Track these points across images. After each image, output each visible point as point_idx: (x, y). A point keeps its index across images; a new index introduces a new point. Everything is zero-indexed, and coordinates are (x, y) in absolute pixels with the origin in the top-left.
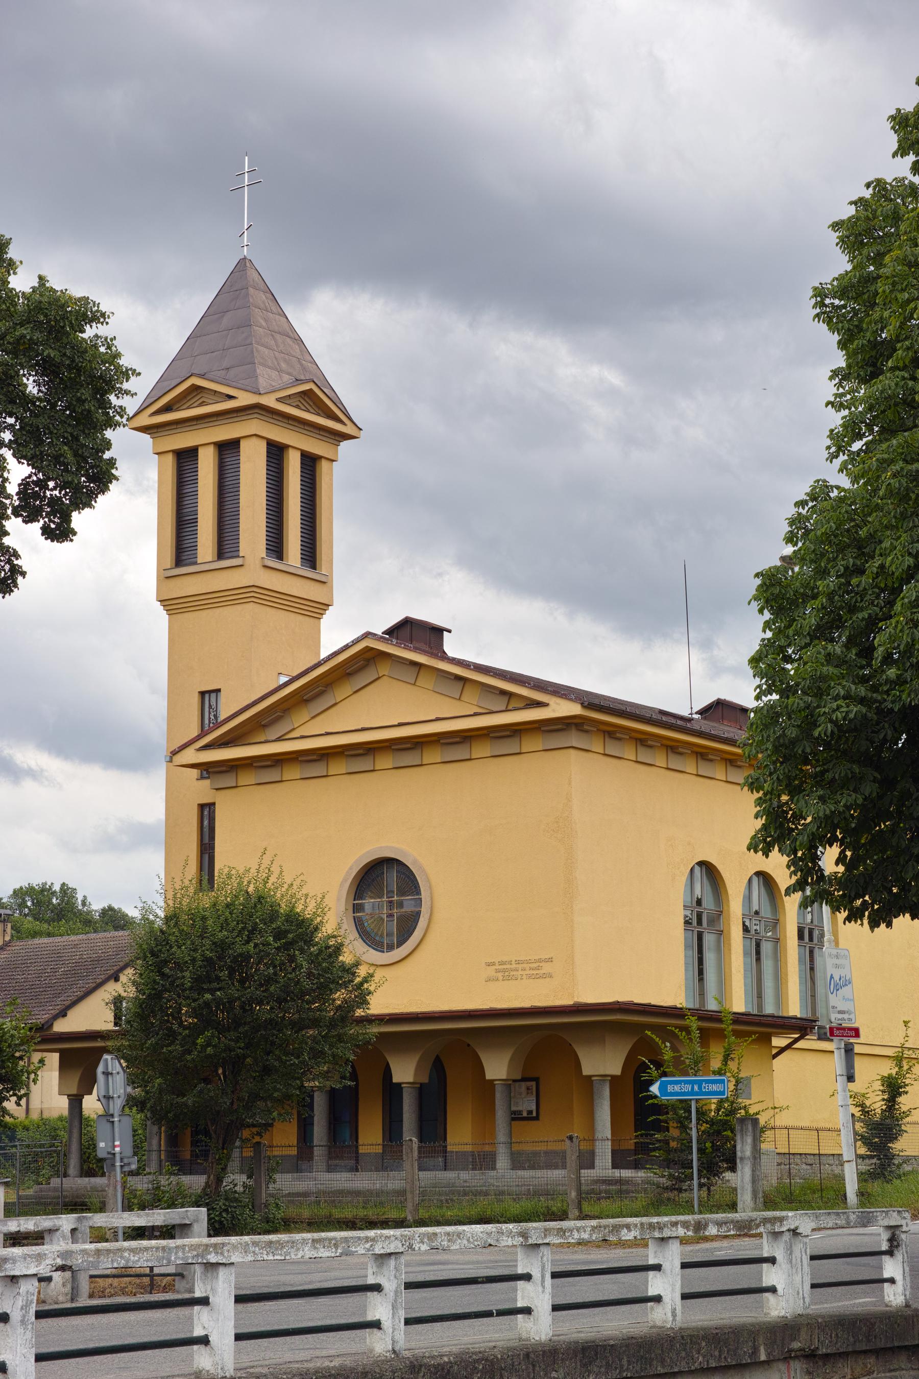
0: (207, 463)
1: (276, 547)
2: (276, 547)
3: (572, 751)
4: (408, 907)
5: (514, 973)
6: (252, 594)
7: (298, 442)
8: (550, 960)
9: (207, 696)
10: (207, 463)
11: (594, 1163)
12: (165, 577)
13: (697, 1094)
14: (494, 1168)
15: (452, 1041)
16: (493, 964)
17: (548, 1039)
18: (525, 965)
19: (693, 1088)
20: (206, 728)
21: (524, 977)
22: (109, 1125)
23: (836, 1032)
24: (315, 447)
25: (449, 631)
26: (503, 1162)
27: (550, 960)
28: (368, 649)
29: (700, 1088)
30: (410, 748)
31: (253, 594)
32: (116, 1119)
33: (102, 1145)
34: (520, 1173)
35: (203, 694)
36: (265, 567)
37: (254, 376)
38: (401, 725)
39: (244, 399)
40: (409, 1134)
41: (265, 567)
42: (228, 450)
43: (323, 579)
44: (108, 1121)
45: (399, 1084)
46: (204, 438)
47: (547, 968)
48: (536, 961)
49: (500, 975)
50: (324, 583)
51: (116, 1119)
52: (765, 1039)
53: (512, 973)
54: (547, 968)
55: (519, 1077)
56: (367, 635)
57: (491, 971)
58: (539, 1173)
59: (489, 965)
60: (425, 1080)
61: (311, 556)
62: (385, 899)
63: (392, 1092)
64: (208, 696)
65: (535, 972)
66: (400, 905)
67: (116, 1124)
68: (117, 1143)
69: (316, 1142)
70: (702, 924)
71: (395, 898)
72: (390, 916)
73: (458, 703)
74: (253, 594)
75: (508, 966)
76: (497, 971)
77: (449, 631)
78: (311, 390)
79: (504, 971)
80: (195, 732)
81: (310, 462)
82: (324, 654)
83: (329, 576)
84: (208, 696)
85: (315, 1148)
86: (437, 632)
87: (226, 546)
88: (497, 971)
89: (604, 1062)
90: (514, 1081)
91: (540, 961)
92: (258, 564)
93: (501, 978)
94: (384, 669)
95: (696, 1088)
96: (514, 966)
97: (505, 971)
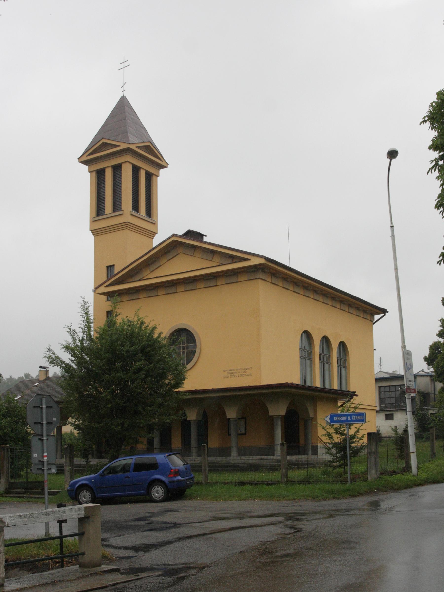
0: (109, 175)
1: (136, 207)
2: (136, 207)
3: (260, 280)
4: (191, 349)
5: (236, 374)
6: (127, 226)
7: (144, 166)
8: (250, 369)
9: (109, 268)
10: (109, 175)
11: (274, 453)
12: (93, 221)
13: (349, 421)
14: (230, 455)
15: (214, 402)
16: (226, 371)
17: (254, 400)
18: (240, 371)
19: (347, 418)
20: (109, 277)
21: (240, 376)
22: (40, 442)
23: (409, 391)
24: (152, 170)
25: (206, 236)
26: (234, 453)
27: (250, 369)
28: (174, 241)
29: (351, 418)
30: (190, 283)
31: (126, 226)
32: (45, 438)
33: (35, 455)
34: (243, 457)
35: (108, 267)
36: (132, 215)
37: (127, 137)
38: (188, 272)
39: (123, 146)
40: (194, 443)
41: (132, 215)
42: (117, 169)
43: (154, 222)
44: (39, 439)
45: (190, 421)
46: (108, 164)
47: (249, 372)
48: (245, 369)
49: (229, 375)
50: (154, 224)
51: (45, 438)
52: (336, 401)
53: (234, 374)
54: (249, 372)
55: (240, 417)
56: (174, 235)
57: (226, 374)
58: (250, 458)
59: (225, 371)
60: (200, 419)
61: (149, 211)
62: (181, 345)
63: (186, 425)
64: (110, 268)
65: (244, 374)
66: (187, 348)
67: (45, 442)
68: (45, 454)
69: (155, 447)
70: (306, 355)
71: (185, 345)
72: (183, 353)
73: (211, 262)
74: (126, 226)
75: (233, 371)
76: (228, 374)
77: (206, 236)
78: (149, 145)
79: (231, 373)
80: (105, 279)
81: (149, 177)
82: (154, 246)
83: (156, 221)
84: (110, 268)
85: (155, 450)
86: (202, 236)
87: (117, 206)
88: (228, 374)
89: (279, 410)
90: (239, 419)
91: (246, 369)
92: (129, 214)
93: (230, 376)
94: (181, 250)
95: (349, 418)
96: (235, 371)
97: (232, 374)
